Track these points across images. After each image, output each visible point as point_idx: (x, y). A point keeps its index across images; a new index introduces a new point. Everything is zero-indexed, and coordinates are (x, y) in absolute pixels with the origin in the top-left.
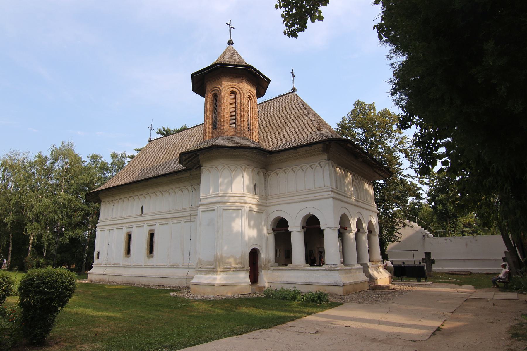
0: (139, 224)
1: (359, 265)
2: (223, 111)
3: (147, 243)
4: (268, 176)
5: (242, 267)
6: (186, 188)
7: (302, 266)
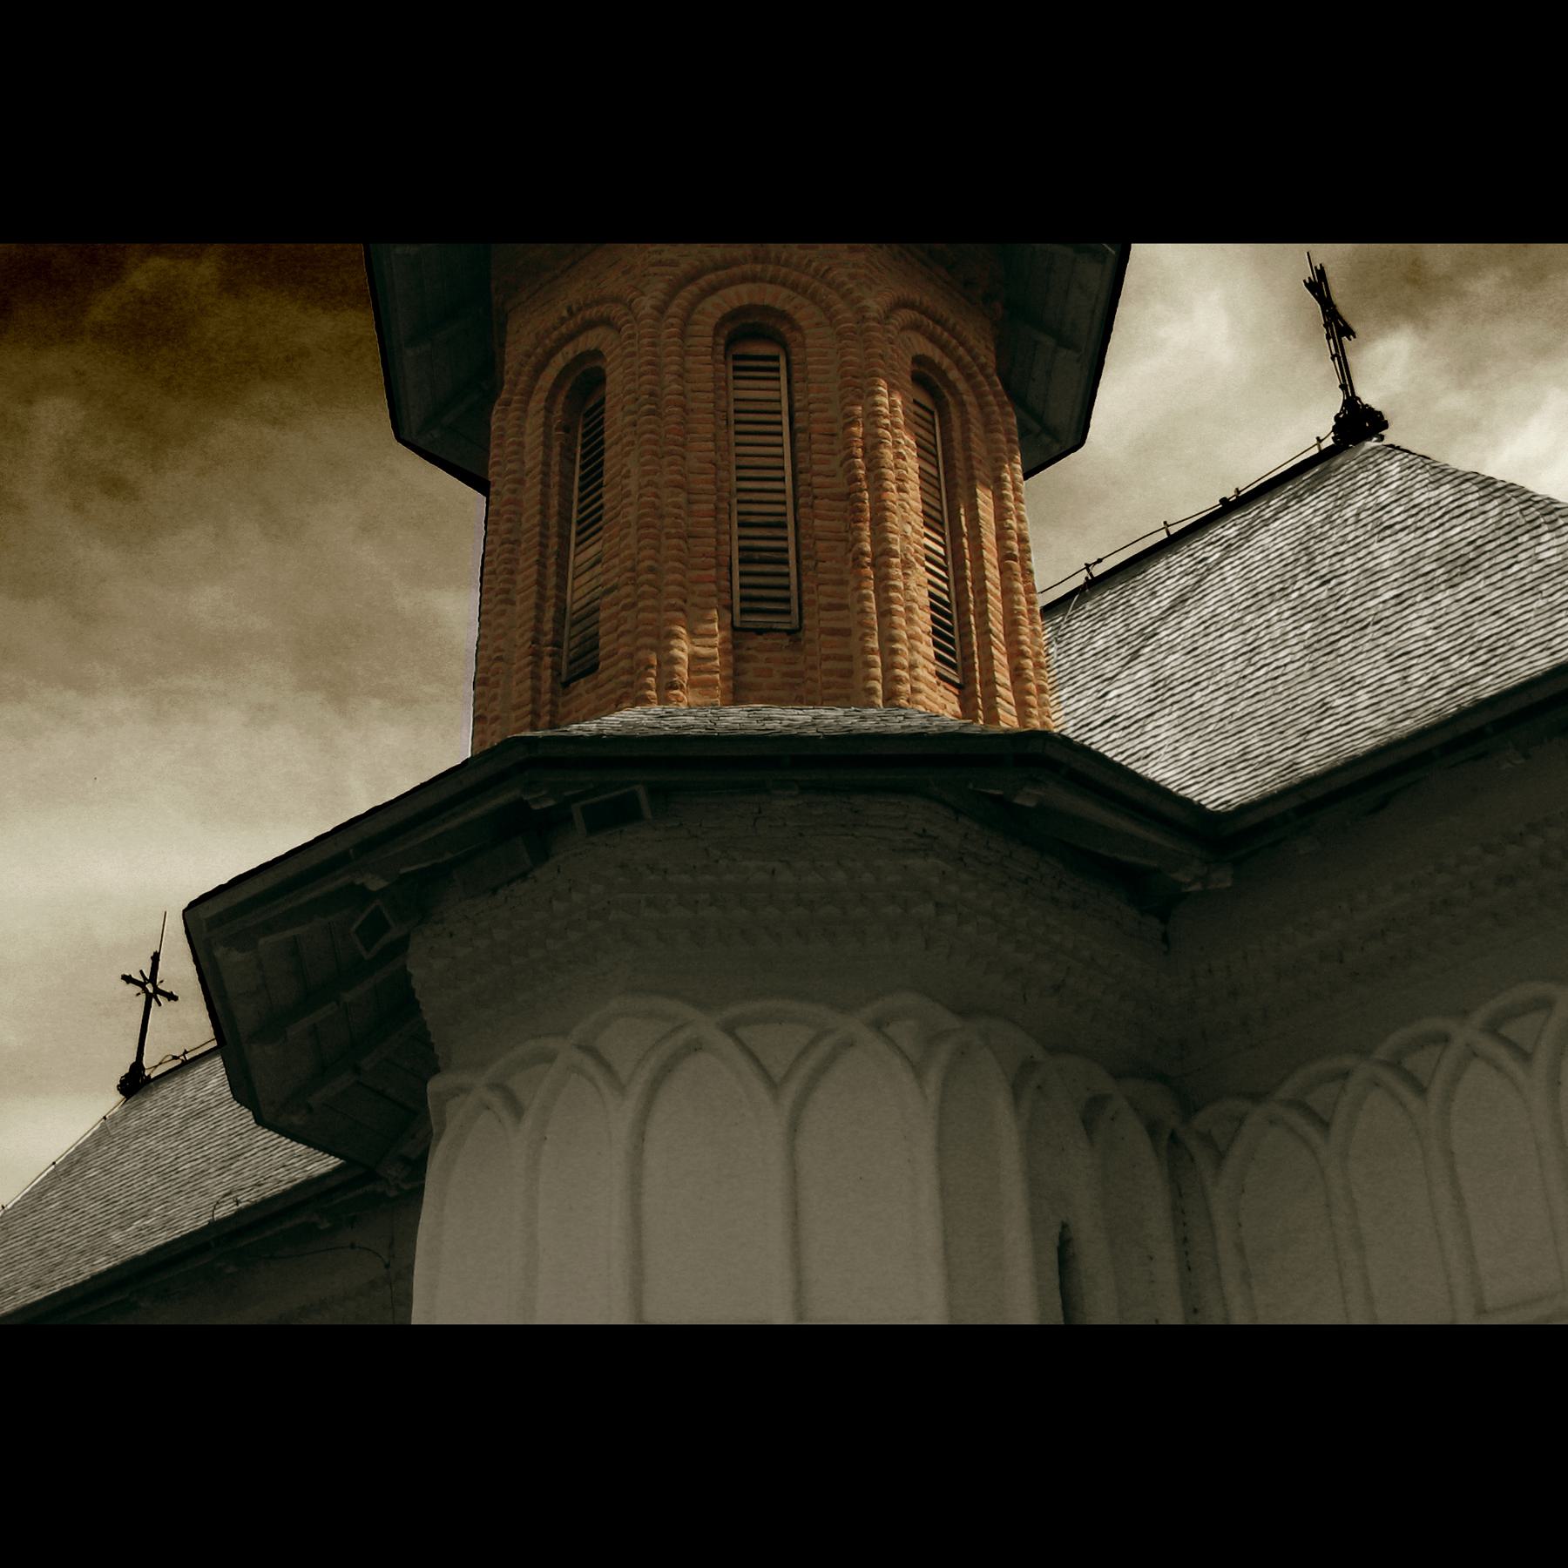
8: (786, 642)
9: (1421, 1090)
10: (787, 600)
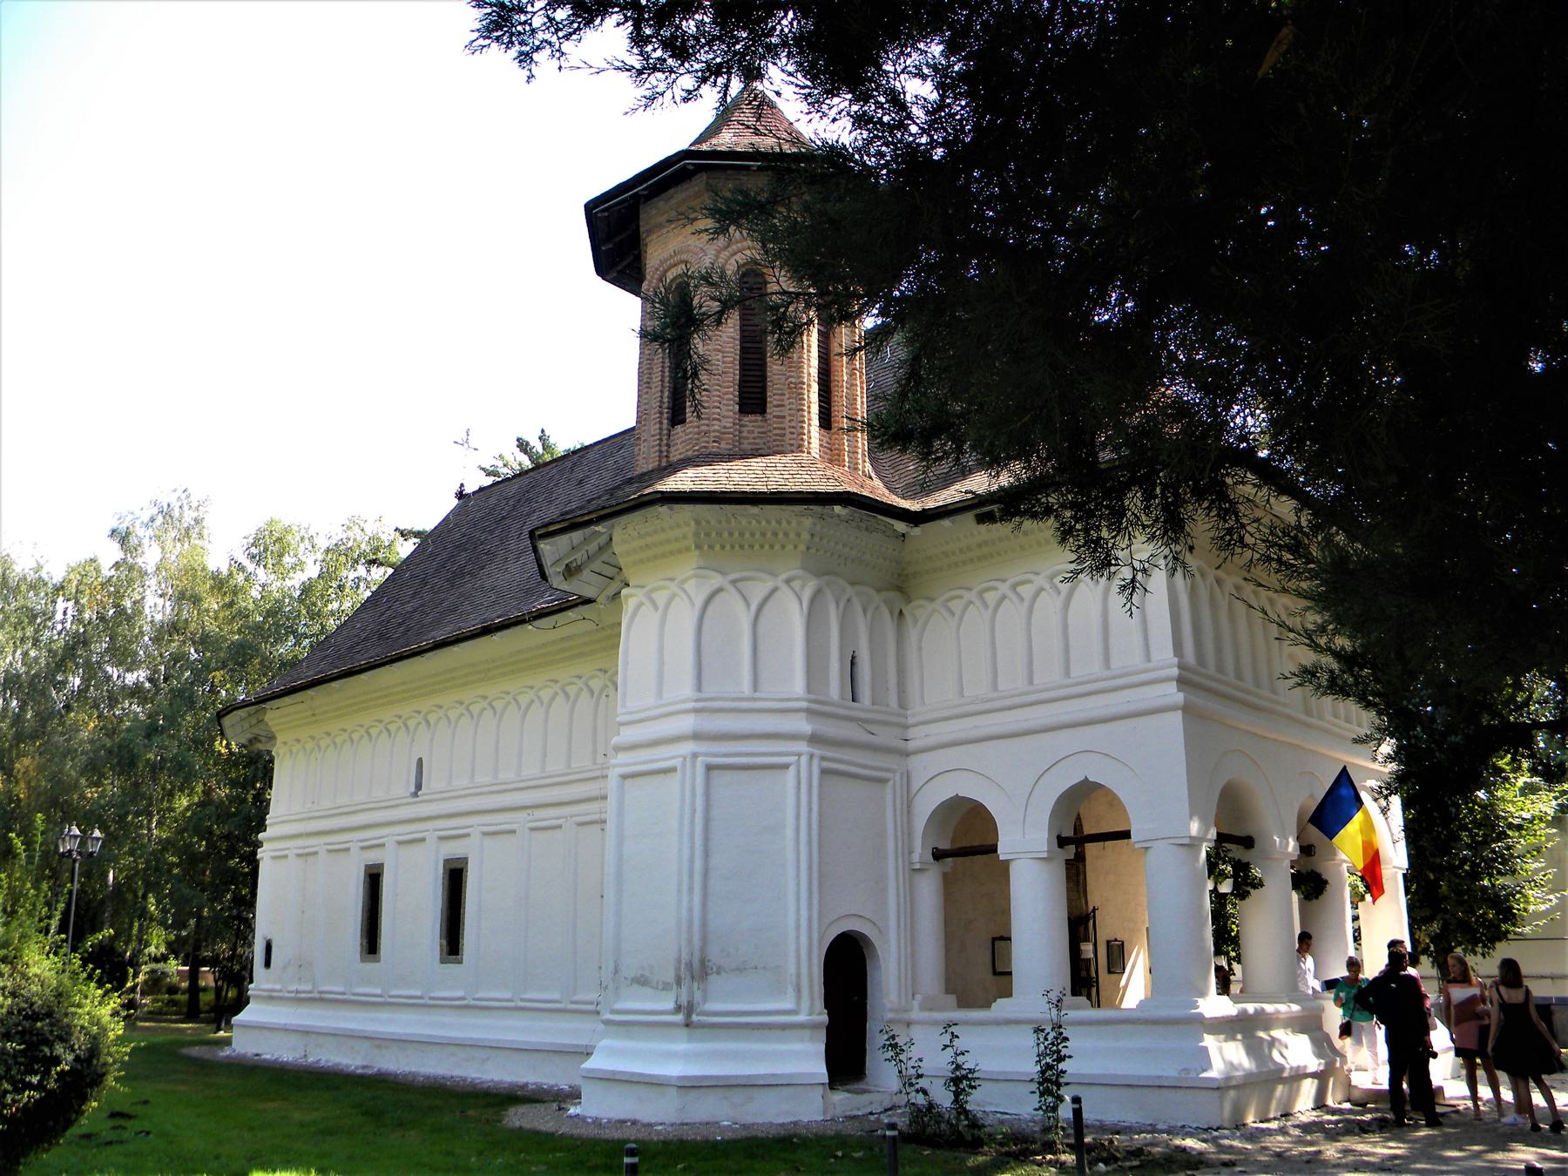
0: (406, 831)
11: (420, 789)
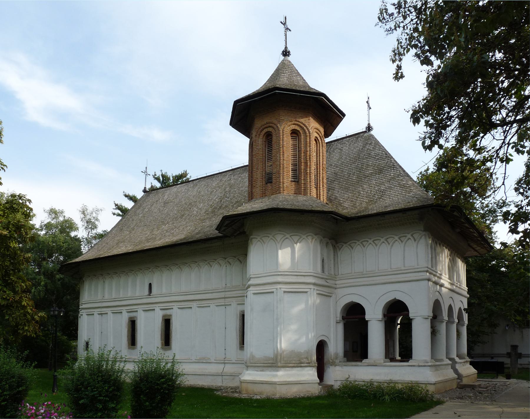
1: (447, 360)
2: (282, 159)
3: (161, 332)
4: (338, 250)
5: (307, 362)
6: (217, 261)
7: (383, 362)
8: (297, 183)
9: (364, 247)
10: (297, 177)
11: (151, 293)
